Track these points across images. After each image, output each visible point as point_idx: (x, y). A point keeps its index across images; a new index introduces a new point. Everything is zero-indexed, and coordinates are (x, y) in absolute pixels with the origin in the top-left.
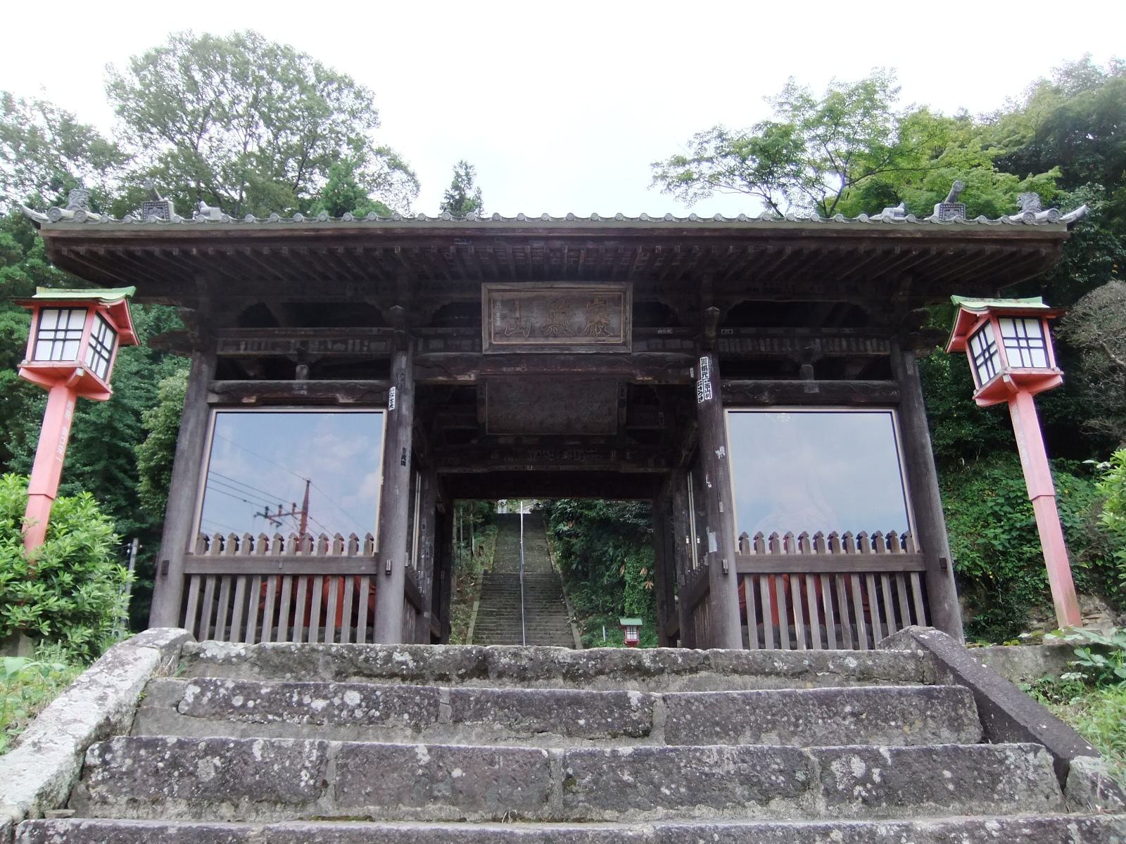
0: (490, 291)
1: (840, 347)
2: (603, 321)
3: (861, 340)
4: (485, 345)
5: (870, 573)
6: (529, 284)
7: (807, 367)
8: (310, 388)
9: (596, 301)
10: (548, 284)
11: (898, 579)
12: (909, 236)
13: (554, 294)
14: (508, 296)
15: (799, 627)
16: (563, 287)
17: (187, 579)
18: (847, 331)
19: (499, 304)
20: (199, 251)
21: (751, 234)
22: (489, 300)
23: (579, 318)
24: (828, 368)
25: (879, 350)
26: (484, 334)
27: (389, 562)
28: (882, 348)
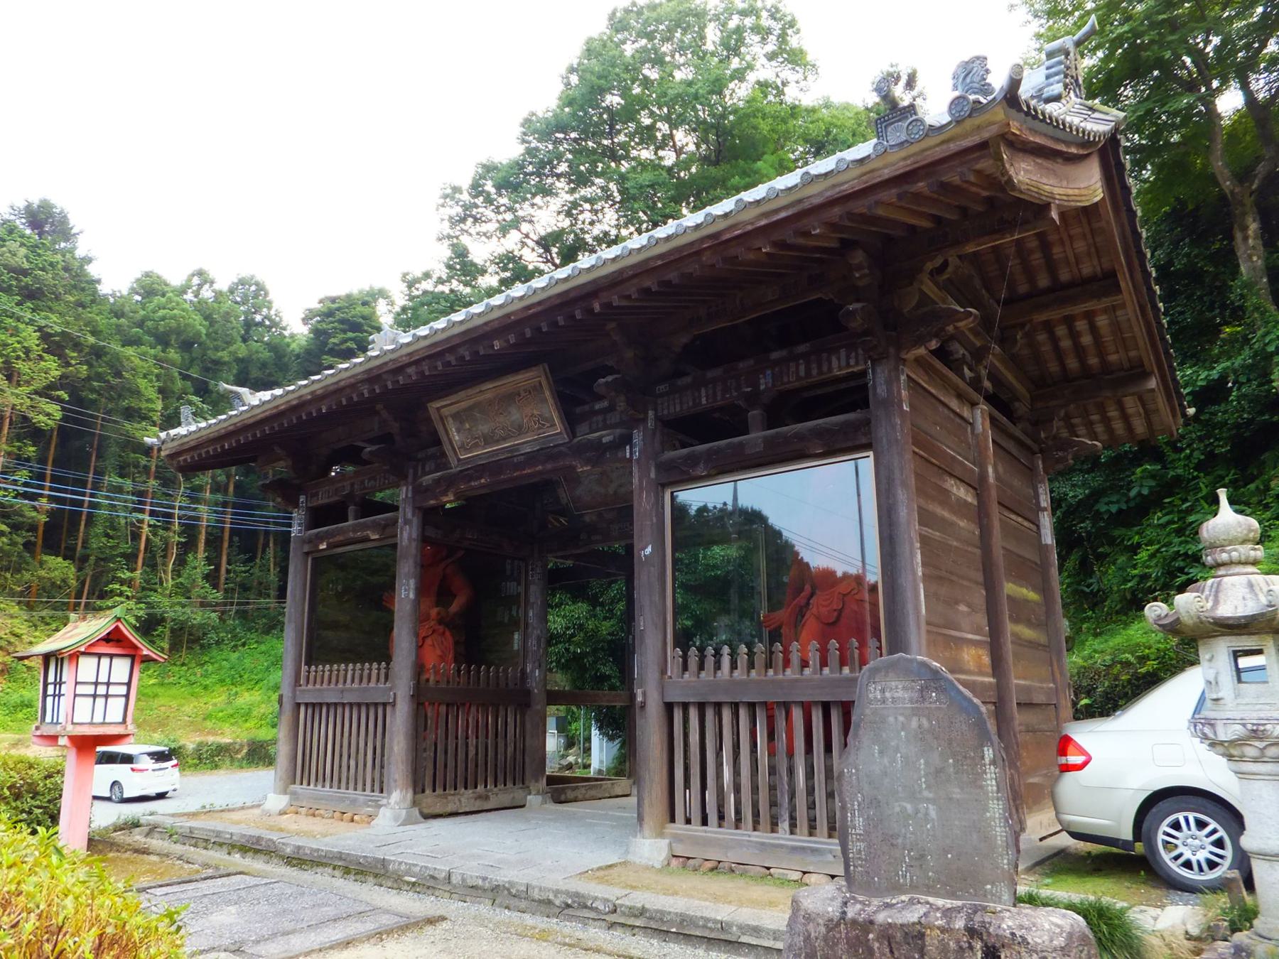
0: (438, 409)
1: (797, 375)
2: (535, 412)
3: (825, 355)
4: (453, 462)
5: (816, 703)
6: (462, 394)
7: (755, 414)
8: (769, 442)
9: (523, 394)
10: (477, 389)
11: (777, 713)
12: (750, 228)
13: (488, 395)
14: (454, 409)
15: (352, 763)
16: (489, 390)
17: (669, 707)
18: (802, 348)
19: (450, 420)
20: (775, 244)
21: (572, 295)
22: (441, 418)
23: (515, 415)
24: (783, 408)
25: (848, 365)
26: (449, 453)
27: (639, 692)
28: (852, 362)
